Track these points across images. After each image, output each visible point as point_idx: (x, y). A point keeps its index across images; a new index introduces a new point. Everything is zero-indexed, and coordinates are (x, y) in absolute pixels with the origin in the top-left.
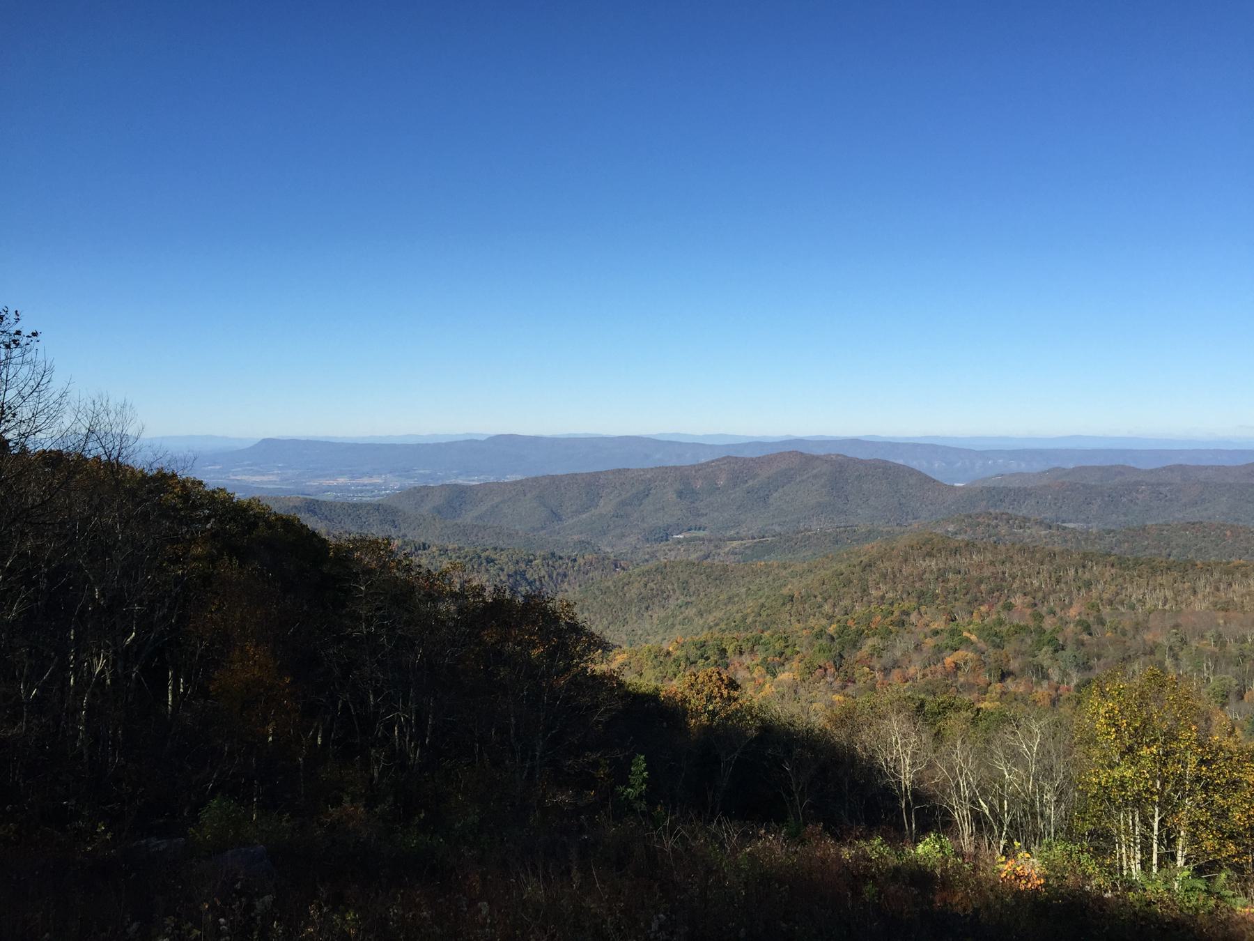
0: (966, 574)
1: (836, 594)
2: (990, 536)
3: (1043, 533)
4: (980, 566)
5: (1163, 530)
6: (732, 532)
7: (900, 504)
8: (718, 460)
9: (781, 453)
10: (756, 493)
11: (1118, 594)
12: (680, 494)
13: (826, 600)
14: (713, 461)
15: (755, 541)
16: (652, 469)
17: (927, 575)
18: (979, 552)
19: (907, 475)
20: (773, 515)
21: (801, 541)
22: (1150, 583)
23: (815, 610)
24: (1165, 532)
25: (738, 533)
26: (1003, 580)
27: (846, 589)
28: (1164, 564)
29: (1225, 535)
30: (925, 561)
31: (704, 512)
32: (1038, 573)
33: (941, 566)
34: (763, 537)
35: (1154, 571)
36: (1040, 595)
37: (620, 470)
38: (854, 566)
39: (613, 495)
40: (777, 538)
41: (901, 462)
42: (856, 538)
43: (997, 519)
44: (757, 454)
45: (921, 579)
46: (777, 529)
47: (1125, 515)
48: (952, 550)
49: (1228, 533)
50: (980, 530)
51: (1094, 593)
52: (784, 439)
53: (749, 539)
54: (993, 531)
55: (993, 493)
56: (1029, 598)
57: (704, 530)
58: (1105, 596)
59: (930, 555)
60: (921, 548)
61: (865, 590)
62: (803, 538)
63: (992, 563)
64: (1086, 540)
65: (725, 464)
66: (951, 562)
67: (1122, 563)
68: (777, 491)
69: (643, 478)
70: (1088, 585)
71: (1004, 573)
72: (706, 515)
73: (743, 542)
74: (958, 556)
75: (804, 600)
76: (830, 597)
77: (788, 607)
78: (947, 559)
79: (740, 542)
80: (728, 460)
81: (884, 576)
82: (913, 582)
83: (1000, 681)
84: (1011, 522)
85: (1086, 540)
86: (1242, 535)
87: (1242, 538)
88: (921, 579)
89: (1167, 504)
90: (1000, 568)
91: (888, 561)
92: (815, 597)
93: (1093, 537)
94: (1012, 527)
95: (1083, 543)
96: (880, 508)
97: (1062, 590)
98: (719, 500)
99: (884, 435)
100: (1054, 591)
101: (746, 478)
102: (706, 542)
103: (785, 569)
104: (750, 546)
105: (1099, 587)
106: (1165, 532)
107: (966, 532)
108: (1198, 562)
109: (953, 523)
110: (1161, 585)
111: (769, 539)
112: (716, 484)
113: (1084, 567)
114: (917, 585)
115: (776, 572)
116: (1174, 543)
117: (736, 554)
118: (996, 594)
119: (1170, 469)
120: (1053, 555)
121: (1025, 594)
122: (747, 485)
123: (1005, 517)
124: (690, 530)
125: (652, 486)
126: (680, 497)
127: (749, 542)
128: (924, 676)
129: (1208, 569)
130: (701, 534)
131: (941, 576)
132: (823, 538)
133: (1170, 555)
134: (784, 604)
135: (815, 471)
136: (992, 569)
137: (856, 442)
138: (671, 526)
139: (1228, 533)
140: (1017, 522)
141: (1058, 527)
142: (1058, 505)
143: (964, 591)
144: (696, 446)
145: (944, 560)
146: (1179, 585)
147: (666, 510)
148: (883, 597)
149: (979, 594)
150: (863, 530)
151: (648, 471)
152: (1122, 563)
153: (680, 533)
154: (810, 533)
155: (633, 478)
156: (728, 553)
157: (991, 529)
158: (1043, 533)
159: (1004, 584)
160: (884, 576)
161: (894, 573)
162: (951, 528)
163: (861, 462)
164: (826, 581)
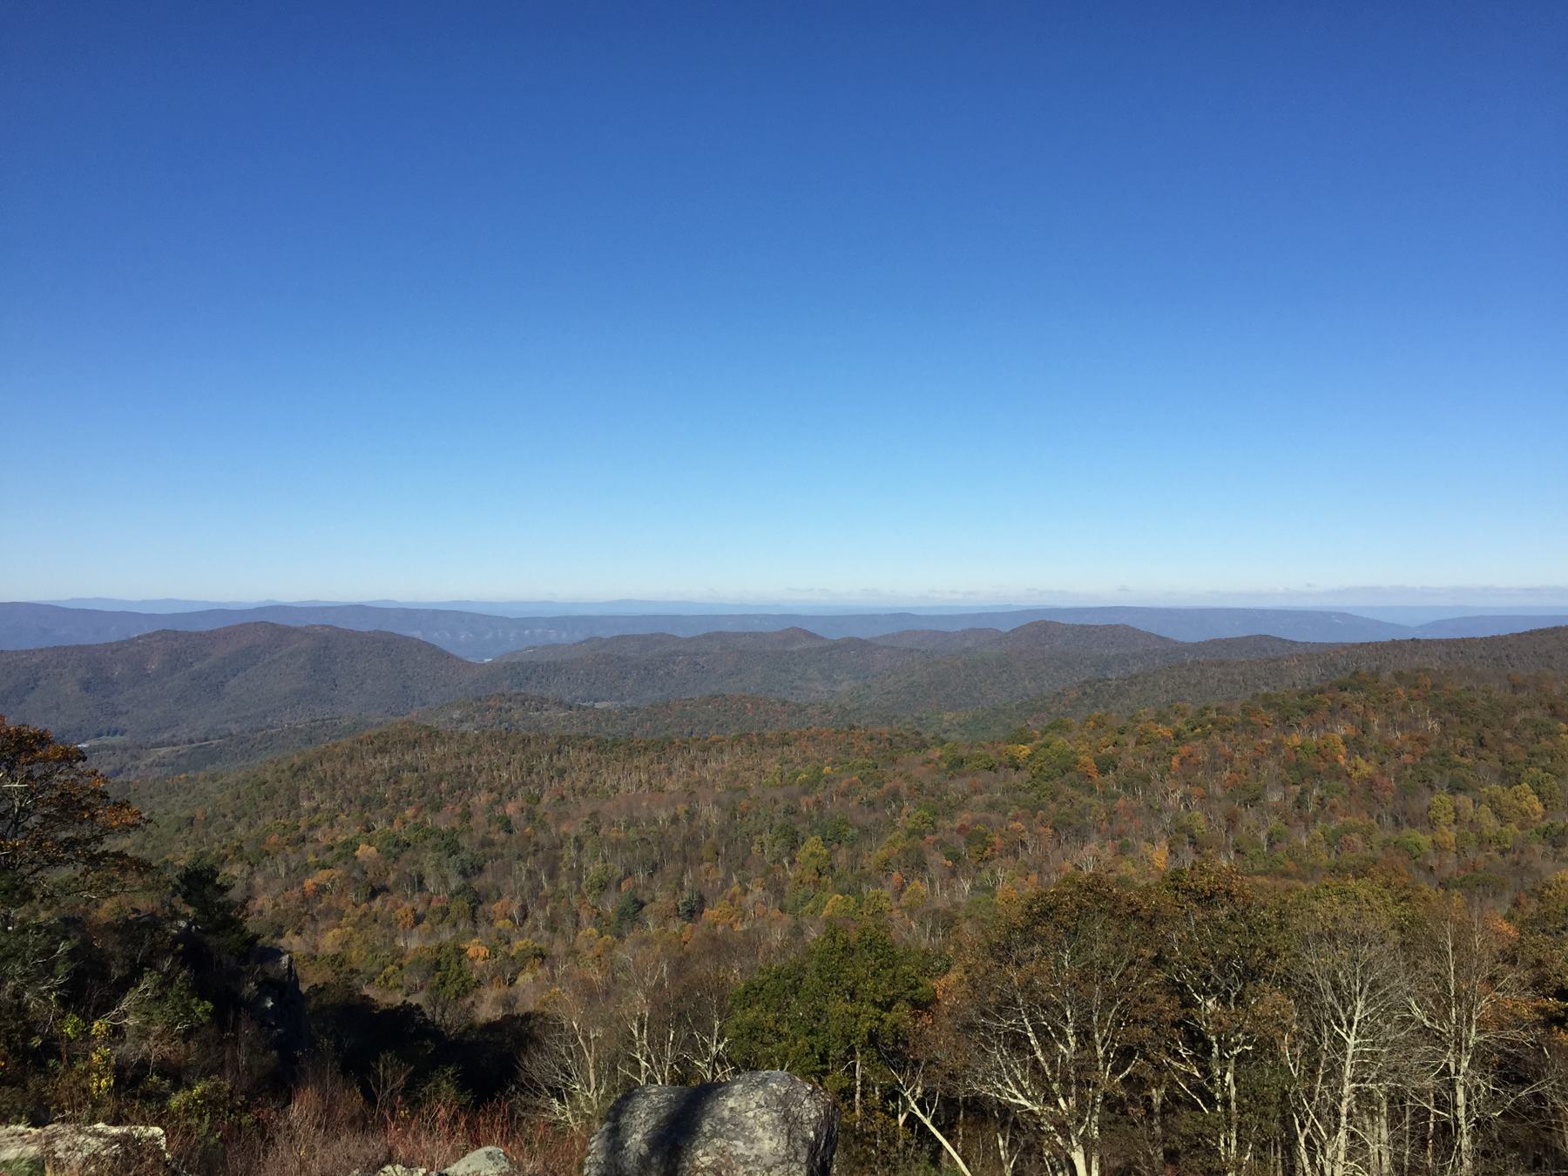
0: (424, 771)
1: (254, 810)
2: (501, 723)
4: (442, 761)
6: (166, 736)
7: (404, 687)
8: (149, 636)
10: (206, 679)
11: (592, 781)
12: (86, 686)
13: (238, 819)
15: (194, 745)
16: (41, 650)
17: (377, 776)
18: (443, 743)
19: (415, 650)
21: (260, 742)
22: (627, 766)
23: (221, 835)
25: (174, 736)
26: (467, 775)
27: (267, 803)
28: (641, 744)
29: (746, 707)
30: (375, 758)
32: (509, 764)
33: (395, 762)
34: (206, 740)
36: (507, 789)
38: (283, 771)
41: (418, 634)
42: (336, 733)
43: (510, 701)
44: (219, 624)
47: (662, 690)
49: (749, 705)
50: (489, 715)
51: (567, 783)
52: (262, 606)
53: (184, 743)
54: (504, 716)
55: (519, 670)
56: (495, 794)
57: (121, 735)
58: (580, 784)
59: (382, 750)
60: (372, 743)
61: (293, 802)
62: (263, 737)
63: (457, 756)
64: (608, 720)
65: (160, 641)
66: (408, 758)
67: (600, 746)
68: (235, 675)
69: (25, 663)
70: (562, 773)
71: (469, 767)
75: (208, 822)
76: (245, 815)
77: (185, 832)
79: (170, 749)
80: (165, 635)
84: (526, 704)
85: (608, 720)
86: (762, 707)
89: (704, 676)
90: (465, 760)
92: (224, 816)
93: (614, 717)
94: (528, 710)
95: (603, 724)
96: (378, 693)
97: (533, 781)
99: (400, 600)
100: (524, 784)
101: (190, 660)
102: (118, 752)
103: (215, 781)
104: (186, 754)
105: (574, 775)
107: (473, 718)
108: (676, 740)
109: (459, 707)
110: (636, 767)
111: (215, 742)
112: (145, 669)
113: (559, 753)
114: (362, 789)
117: (164, 765)
118: (458, 792)
119: (709, 637)
120: (526, 742)
121: (491, 791)
123: (519, 697)
125: (40, 675)
126: (87, 689)
127: (184, 749)
128: (276, 905)
129: (685, 747)
131: (394, 776)
134: (179, 830)
136: (456, 763)
137: (361, 610)
139: (749, 705)
140: (533, 703)
142: (592, 680)
143: (420, 793)
145: (400, 755)
146: (655, 767)
148: (316, 810)
149: (437, 795)
151: (34, 653)
152: (600, 746)
154: (273, 731)
155: (9, 663)
156: (152, 765)
157: (503, 714)
159: (468, 780)
160: (321, 782)
161: (333, 776)
162: (456, 715)
163: (355, 634)
164: (242, 794)
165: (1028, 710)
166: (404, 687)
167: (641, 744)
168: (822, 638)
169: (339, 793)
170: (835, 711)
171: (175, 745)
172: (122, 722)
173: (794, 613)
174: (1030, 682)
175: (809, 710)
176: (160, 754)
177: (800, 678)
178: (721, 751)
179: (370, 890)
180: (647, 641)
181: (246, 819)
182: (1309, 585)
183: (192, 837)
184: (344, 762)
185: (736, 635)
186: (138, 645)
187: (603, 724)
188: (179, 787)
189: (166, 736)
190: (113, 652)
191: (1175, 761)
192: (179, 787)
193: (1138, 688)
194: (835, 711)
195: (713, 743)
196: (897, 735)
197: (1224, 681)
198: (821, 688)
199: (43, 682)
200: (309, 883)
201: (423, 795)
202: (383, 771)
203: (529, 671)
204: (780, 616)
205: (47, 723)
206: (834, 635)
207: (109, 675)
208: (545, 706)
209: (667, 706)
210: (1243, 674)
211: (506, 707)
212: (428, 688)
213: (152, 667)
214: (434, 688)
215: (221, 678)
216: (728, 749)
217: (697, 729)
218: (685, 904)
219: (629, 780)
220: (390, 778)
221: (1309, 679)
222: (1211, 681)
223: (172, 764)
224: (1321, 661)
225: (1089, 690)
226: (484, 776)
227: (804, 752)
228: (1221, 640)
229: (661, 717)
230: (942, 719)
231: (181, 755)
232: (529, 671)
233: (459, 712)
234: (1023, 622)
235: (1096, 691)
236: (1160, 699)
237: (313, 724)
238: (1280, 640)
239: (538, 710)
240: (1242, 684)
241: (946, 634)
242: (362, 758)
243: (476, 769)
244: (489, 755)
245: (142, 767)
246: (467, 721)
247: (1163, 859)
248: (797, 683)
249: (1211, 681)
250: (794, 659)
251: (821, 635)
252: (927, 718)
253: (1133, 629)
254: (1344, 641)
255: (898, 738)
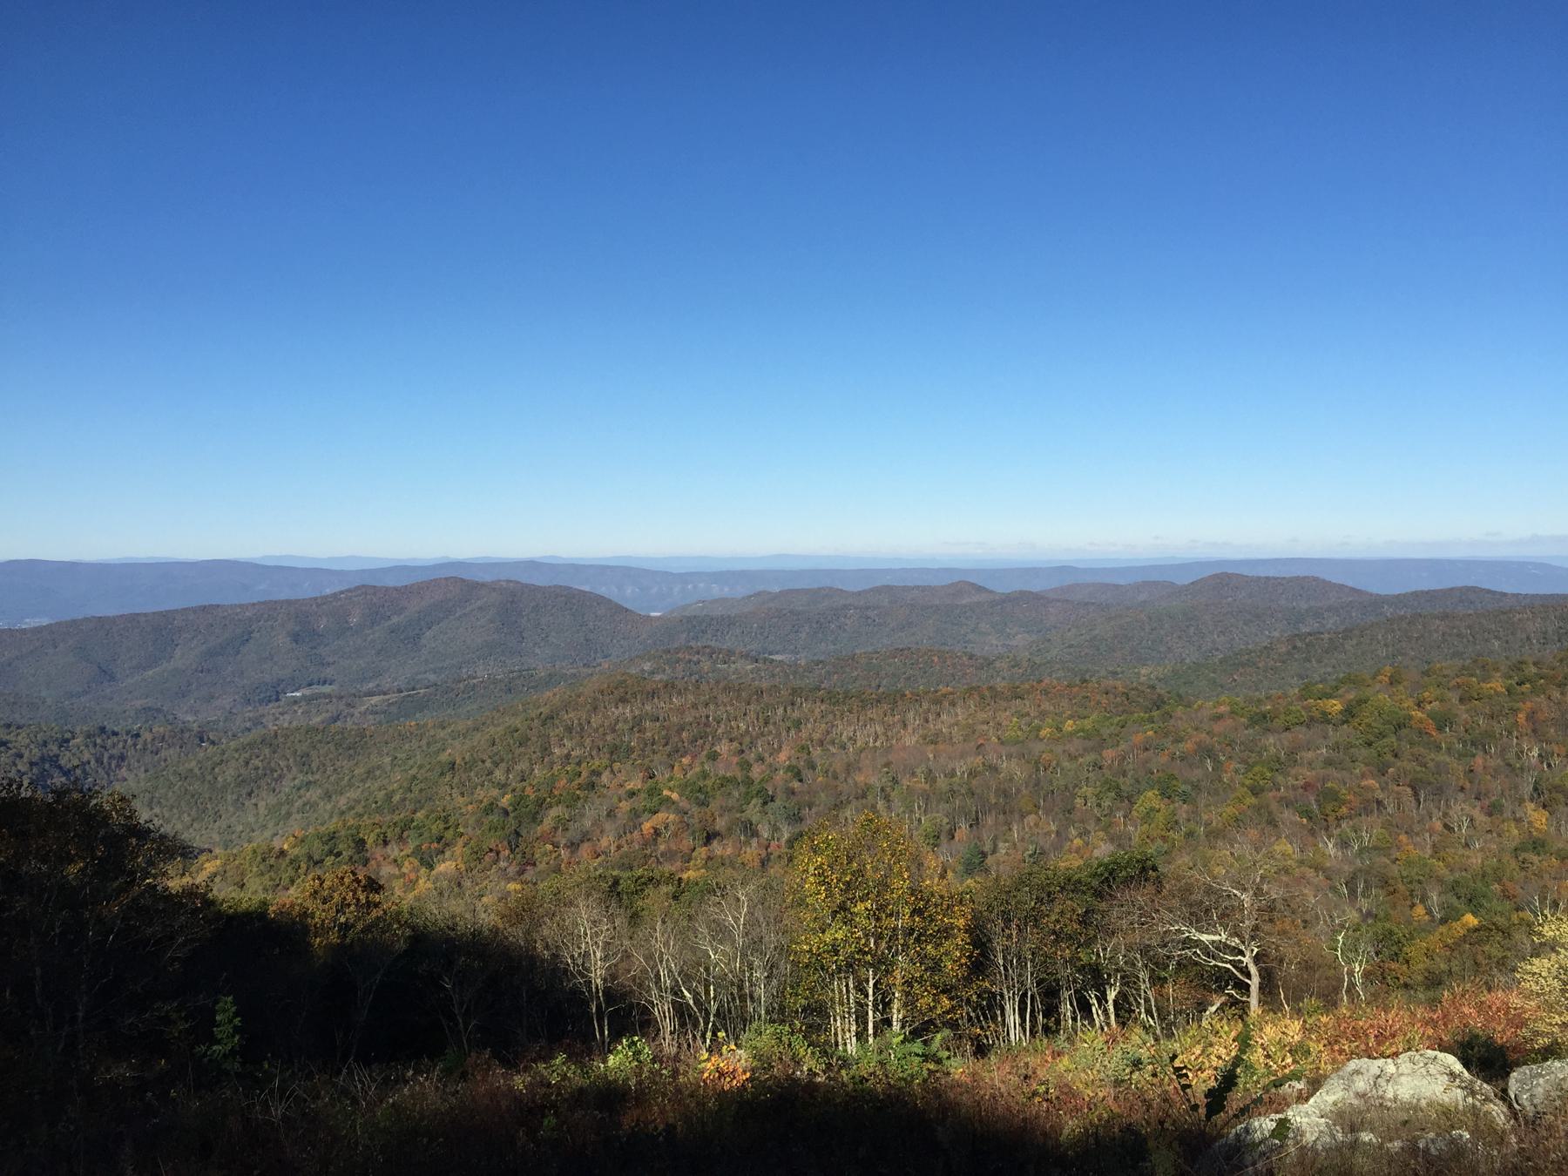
0: (665, 720)
1: (510, 756)
2: (691, 675)
3: (749, 667)
4: (681, 711)
5: (872, 659)
6: (371, 685)
7: (587, 640)
8: (349, 590)
9: (435, 580)
10: (403, 631)
11: (828, 733)
12: (296, 638)
13: (497, 765)
14: (342, 592)
15: (402, 695)
16: (254, 604)
18: (679, 693)
20: (426, 660)
21: (463, 692)
24: (874, 661)
25: (378, 685)
27: (522, 749)
28: (873, 696)
29: (933, 661)
30: (618, 708)
31: (331, 660)
32: (745, 715)
35: (864, 704)
36: (747, 739)
37: (205, 607)
38: (533, 720)
39: (195, 642)
40: (432, 690)
41: (586, 588)
43: (698, 653)
45: (614, 731)
46: (432, 677)
48: (649, 693)
49: (936, 659)
50: (679, 667)
51: (804, 734)
53: (394, 693)
54: (694, 668)
55: (694, 623)
57: (330, 684)
58: (816, 736)
59: (623, 700)
60: (612, 693)
63: (694, 706)
64: (795, 673)
66: (648, 707)
67: (831, 698)
69: (240, 617)
70: (798, 724)
71: (708, 717)
72: (334, 663)
73: (387, 697)
74: (656, 700)
75: (469, 766)
76: (502, 760)
78: (643, 704)
79: (382, 697)
80: (364, 590)
81: (569, 729)
82: (604, 734)
83: (705, 845)
85: (795, 673)
87: (948, 663)
88: (614, 731)
89: (876, 629)
90: (703, 711)
91: (574, 710)
92: (483, 762)
95: (791, 677)
98: (351, 643)
100: (762, 735)
101: (388, 614)
102: (334, 700)
103: (444, 728)
104: (396, 702)
106: (874, 661)
108: (907, 692)
109: (649, 660)
110: (871, 719)
111: (422, 691)
112: (347, 622)
114: (609, 738)
115: (432, 733)
116: (883, 672)
118: (700, 742)
119: (877, 590)
121: (731, 740)
122: (390, 622)
123: (708, 650)
124: (310, 685)
126: (296, 642)
127: (393, 697)
129: (917, 699)
130: (327, 689)
131: (637, 724)
132: (492, 686)
133: (879, 686)
134: (442, 774)
135: (479, 603)
136: (693, 712)
137: (532, 565)
138: (283, 681)
139: (936, 659)
141: (765, 660)
142: (766, 634)
143: (663, 741)
144: (315, 573)
147: (275, 659)
148: (568, 756)
150: (543, 674)
152: (831, 698)
153: (297, 690)
154: (475, 681)
156: (365, 713)
158: (749, 667)
160: (569, 729)
161: (581, 724)
162: (647, 666)
164: (497, 740)
165: (1234, 664)
166: (587, 640)
167: (873, 696)
168: (991, 592)
169: (588, 741)
170: (1025, 664)
171: (385, 694)
172: (329, 672)
173: (863, 567)
174: (1218, 637)
175: (998, 664)
176: (372, 702)
177: (973, 631)
178: (953, 704)
179: (705, 835)
180: (816, 594)
181: (503, 765)
182: (1157, 538)
183: (456, 780)
184: (588, 711)
185: (905, 589)
186: (340, 599)
187: (791, 677)
188: (411, 734)
189: (371, 685)
190: (318, 606)
191: (1521, 717)
192: (411, 734)
193: (1354, 642)
194: (1025, 664)
195: (944, 696)
196: (1133, 689)
197: (1450, 635)
198: (994, 642)
199: (256, 635)
200: (647, 826)
201: (666, 744)
202: (626, 721)
203: (705, 625)
204: (938, 570)
205: (262, 672)
206: (1002, 588)
207: (315, 628)
208: (732, 658)
209: (853, 659)
210: (1469, 627)
211: (695, 659)
212: (609, 640)
213: (354, 620)
214: (615, 641)
215: (417, 631)
216: (960, 703)
217: (884, 682)
218: (1030, 856)
219: (865, 732)
220: (633, 727)
221: (1545, 633)
222: (1435, 635)
223: (385, 712)
224: (1557, 613)
225: (1299, 644)
226: (723, 726)
227: (1039, 706)
228: (1422, 592)
229: (848, 670)
230: (1138, 673)
231: (392, 703)
232: (705, 625)
233: (649, 664)
234: (956, 579)
235: (1307, 645)
236: (1379, 652)
237: (511, 675)
238: (1489, 591)
239: (725, 663)
240: (1471, 638)
241: (1117, 587)
242: (605, 708)
243: (714, 719)
244: (725, 705)
245: (357, 714)
246: (658, 673)
247: (1544, 820)
248: (971, 636)
249: (1435, 635)
250: (966, 612)
251: (991, 588)
252: (1122, 673)
253: (1324, 581)
254: (1541, 592)
255: (1133, 692)
